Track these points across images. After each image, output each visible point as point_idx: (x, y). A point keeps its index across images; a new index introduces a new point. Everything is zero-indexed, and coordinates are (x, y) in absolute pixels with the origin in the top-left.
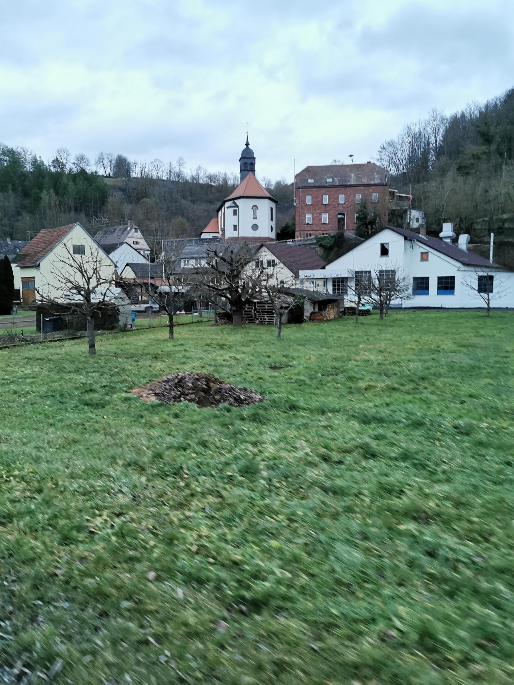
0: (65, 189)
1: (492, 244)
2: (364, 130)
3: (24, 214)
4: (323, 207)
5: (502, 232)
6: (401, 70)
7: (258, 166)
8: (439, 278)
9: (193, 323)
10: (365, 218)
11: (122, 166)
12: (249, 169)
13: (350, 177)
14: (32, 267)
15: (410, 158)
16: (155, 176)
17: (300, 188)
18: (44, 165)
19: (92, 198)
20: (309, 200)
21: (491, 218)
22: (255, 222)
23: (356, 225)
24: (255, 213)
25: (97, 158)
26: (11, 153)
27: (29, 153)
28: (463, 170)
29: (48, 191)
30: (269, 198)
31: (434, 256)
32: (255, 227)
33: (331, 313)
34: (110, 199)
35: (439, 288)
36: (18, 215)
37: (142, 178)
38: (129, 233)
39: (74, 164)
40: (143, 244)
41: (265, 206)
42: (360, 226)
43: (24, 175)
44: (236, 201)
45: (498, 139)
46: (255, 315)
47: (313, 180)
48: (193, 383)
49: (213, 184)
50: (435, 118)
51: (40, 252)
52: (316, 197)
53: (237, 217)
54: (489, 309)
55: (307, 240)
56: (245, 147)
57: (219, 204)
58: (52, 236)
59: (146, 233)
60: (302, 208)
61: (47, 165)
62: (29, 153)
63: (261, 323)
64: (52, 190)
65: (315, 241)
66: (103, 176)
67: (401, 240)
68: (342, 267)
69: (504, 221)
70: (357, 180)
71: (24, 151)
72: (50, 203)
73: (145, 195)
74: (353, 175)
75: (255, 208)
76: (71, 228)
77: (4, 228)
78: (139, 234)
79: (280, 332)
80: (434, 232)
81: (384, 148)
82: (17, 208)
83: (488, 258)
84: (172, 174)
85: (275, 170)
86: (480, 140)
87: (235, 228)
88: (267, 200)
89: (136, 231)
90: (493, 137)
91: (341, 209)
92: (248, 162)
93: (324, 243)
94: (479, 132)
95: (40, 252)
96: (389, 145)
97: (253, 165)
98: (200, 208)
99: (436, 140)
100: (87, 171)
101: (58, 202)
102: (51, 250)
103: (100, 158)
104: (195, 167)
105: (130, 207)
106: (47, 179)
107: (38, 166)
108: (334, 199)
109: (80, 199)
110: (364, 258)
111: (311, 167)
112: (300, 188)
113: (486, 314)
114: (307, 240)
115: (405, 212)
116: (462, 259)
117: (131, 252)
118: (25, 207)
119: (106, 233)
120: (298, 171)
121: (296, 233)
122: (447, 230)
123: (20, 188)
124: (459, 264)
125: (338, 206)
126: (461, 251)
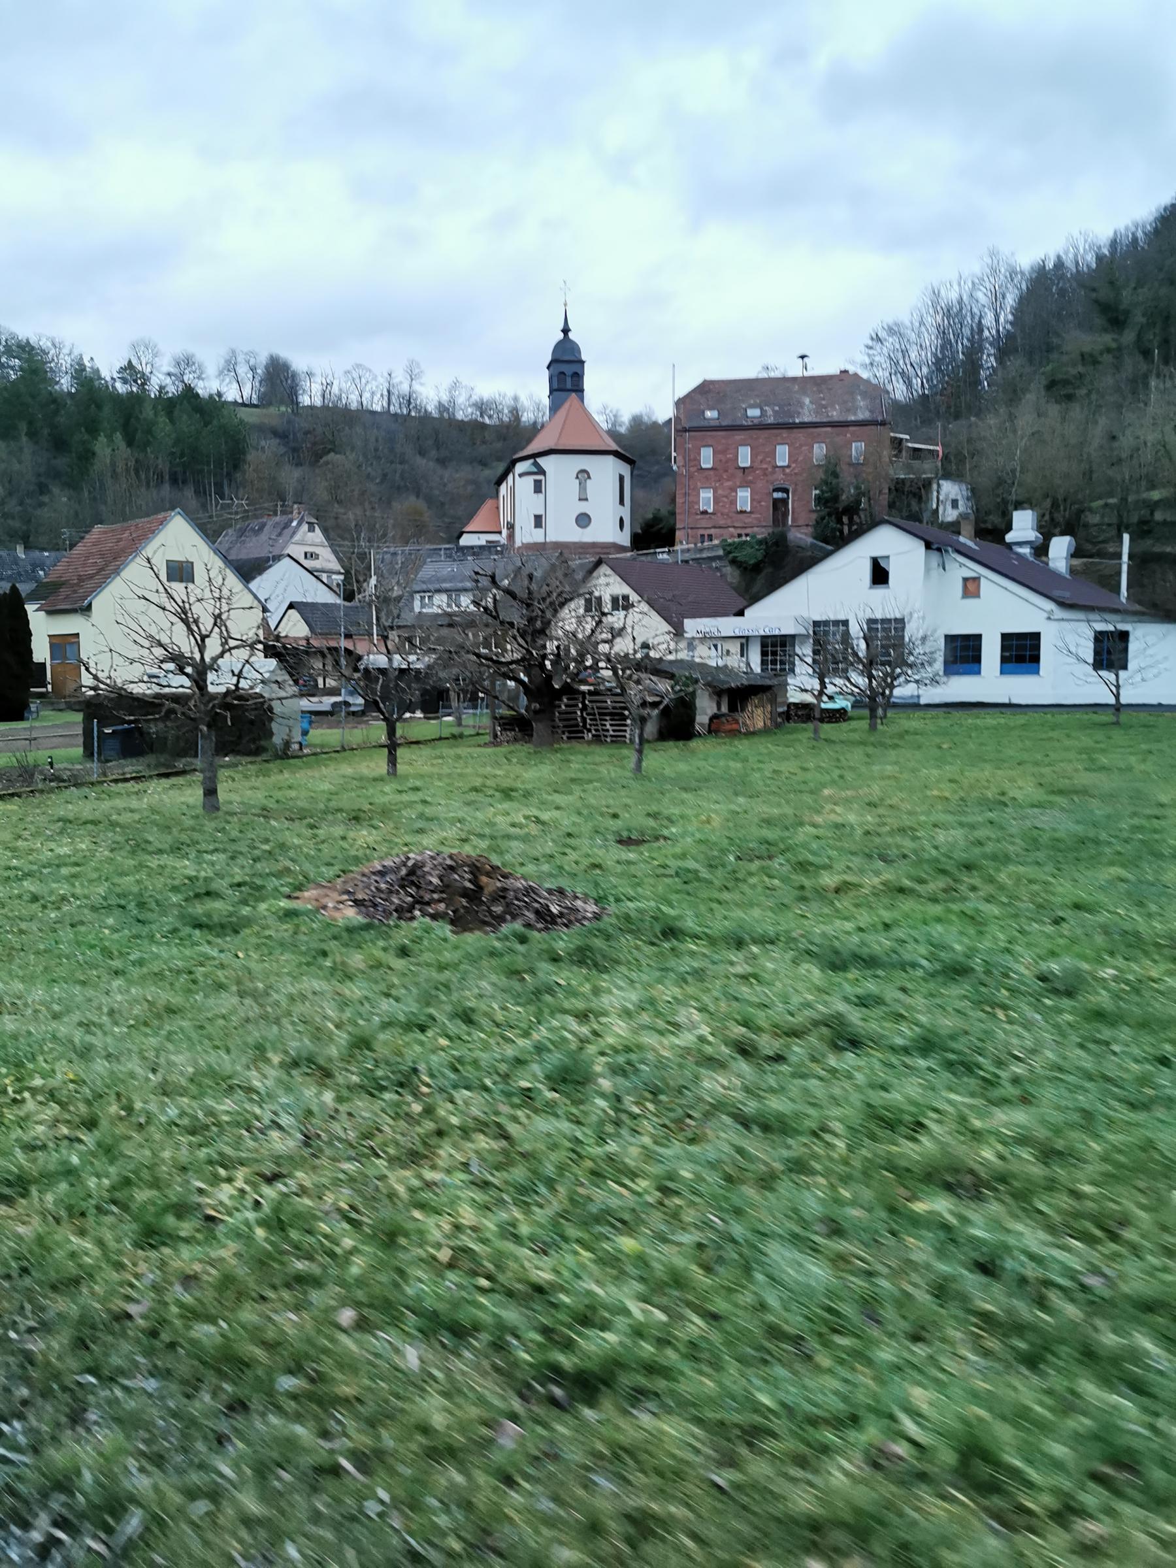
0: (149, 431)
1: (1125, 558)
2: (832, 297)
3: (56, 490)
4: (740, 473)
5: (1149, 532)
6: (917, 160)
7: (591, 381)
8: (1005, 637)
9: (440, 739)
10: (836, 498)
11: (279, 379)
12: (569, 386)
13: (802, 405)
14: (73, 611)
15: (938, 362)
16: (354, 403)
17: (685, 430)
18: (100, 378)
19: (210, 453)
20: (707, 458)
21: (1124, 500)
22: (583, 507)
23: (814, 516)
24: (583, 487)
25: (222, 362)
26: (25, 350)
27: (66, 351)
28: (1060, 389)
29: (110, 438)
30: (616, 454)
31: (993, 587)
32: (583, 520)
33: (757, 716)
34: (251, 456)
35: (1004, 660)
36: (42, 493)
37: (325, 407)
38: (294, 533)
39: (169, 374)
40: (327, 559)
41: (607, 473)
42: (823, 518)
43: (54, 401)
44: (540, 460)
45: (1139, 318)
46: (584, 720)
47: (716, 411)
48: (441, 878)
49: (487, 421)
50: (994, 271)
51: (91, 577)
52: (724, 452)
53: (541, 496)
54: (1118, 707)
55: (701, 550)
56: (561, 335)
57: (501, 467)
58: (120, 540)
59: (334, 533)
60: (691, 477)
61: (108, 379)
62: (66, 351)
63: (598, 740)
64: (118, 436)
65: (721, 552)
66: (235, 403)
67: (917, 548)
68: (784, 610)
69: (1153, 506)
70: (817, 413)
71: (54, 345)
72: (113, 464)
73: (332, 447)
74: (807, 401)
75: (583, 475)
76: (162, 523)
77: (10, 522)
78: (318, 536)
79: (640, 761)
80: (992, 531)
81: (879, 339)
82: (39, 475)
83: (1117, 590)
84: (393, 399)
85: (630, 390)
86: (1099, 321)
87: (538, 521)
88: (611, 458)
89: (311, 529)
90: (1127, 313)
91: (779, 479)
92: (566, 371)
93: (740, 555)
94: (1096, 301)
95: (91, 577)
96: (891, 331)
97: (578, 377)
98: (457, 477)
99: (996, 320)
100: (200, 392)
101: (132, 464)
102: (117, 572)
103: (228, 362)
104: (446, 383)
105: (297, 473)
106: (107, 410)
107: (86, 379)
108: (764, 455)
109: (182, 455)
110: (832, 591)
111: (712, 382)
112: (685, 430)
113: (1112, 718)
114: (701, 550)
115: (927, 484)
116: (1056, 593)
117: (299, 576)
118: (56, 475)
119: (242, 533)
120: (682, 392)
121: (678, 533)
122: (1023, 526)
123: (46, 431)
124: (1049, 605)
125: (773, 473)
126: (1055, 574)
